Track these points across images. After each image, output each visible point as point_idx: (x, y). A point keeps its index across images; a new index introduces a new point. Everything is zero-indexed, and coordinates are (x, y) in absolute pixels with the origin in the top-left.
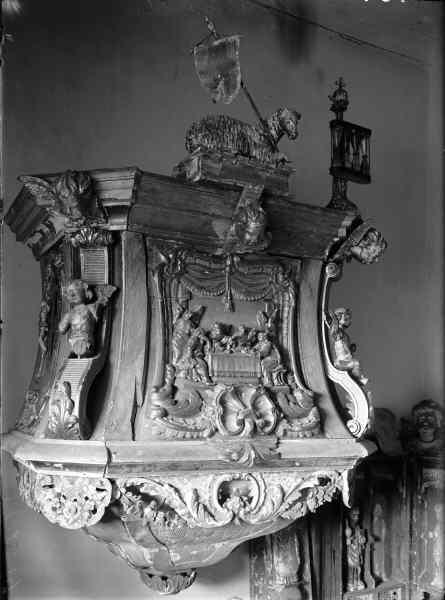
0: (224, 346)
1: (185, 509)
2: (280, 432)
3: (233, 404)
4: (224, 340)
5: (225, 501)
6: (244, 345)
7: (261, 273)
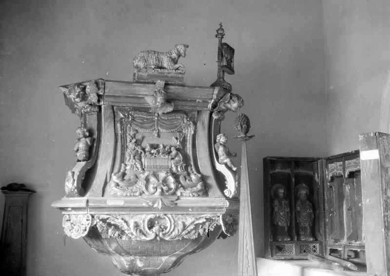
0: (152, 154)
1: (130, 230)
2: (179, 193)
3: (153, 179)
4: (152, 152)
5: (152, 228)
6: (163, 153)
7: (175, 119)
